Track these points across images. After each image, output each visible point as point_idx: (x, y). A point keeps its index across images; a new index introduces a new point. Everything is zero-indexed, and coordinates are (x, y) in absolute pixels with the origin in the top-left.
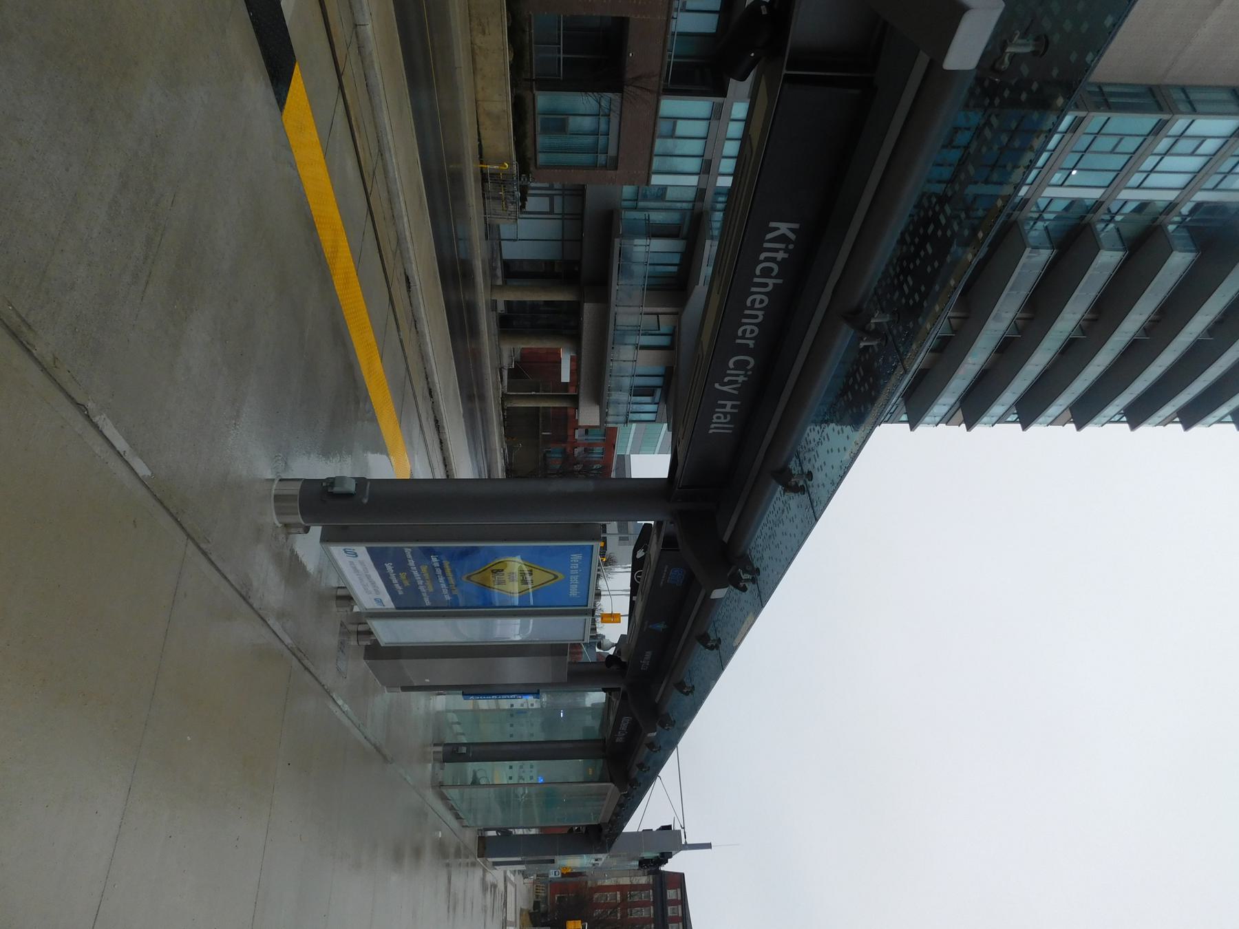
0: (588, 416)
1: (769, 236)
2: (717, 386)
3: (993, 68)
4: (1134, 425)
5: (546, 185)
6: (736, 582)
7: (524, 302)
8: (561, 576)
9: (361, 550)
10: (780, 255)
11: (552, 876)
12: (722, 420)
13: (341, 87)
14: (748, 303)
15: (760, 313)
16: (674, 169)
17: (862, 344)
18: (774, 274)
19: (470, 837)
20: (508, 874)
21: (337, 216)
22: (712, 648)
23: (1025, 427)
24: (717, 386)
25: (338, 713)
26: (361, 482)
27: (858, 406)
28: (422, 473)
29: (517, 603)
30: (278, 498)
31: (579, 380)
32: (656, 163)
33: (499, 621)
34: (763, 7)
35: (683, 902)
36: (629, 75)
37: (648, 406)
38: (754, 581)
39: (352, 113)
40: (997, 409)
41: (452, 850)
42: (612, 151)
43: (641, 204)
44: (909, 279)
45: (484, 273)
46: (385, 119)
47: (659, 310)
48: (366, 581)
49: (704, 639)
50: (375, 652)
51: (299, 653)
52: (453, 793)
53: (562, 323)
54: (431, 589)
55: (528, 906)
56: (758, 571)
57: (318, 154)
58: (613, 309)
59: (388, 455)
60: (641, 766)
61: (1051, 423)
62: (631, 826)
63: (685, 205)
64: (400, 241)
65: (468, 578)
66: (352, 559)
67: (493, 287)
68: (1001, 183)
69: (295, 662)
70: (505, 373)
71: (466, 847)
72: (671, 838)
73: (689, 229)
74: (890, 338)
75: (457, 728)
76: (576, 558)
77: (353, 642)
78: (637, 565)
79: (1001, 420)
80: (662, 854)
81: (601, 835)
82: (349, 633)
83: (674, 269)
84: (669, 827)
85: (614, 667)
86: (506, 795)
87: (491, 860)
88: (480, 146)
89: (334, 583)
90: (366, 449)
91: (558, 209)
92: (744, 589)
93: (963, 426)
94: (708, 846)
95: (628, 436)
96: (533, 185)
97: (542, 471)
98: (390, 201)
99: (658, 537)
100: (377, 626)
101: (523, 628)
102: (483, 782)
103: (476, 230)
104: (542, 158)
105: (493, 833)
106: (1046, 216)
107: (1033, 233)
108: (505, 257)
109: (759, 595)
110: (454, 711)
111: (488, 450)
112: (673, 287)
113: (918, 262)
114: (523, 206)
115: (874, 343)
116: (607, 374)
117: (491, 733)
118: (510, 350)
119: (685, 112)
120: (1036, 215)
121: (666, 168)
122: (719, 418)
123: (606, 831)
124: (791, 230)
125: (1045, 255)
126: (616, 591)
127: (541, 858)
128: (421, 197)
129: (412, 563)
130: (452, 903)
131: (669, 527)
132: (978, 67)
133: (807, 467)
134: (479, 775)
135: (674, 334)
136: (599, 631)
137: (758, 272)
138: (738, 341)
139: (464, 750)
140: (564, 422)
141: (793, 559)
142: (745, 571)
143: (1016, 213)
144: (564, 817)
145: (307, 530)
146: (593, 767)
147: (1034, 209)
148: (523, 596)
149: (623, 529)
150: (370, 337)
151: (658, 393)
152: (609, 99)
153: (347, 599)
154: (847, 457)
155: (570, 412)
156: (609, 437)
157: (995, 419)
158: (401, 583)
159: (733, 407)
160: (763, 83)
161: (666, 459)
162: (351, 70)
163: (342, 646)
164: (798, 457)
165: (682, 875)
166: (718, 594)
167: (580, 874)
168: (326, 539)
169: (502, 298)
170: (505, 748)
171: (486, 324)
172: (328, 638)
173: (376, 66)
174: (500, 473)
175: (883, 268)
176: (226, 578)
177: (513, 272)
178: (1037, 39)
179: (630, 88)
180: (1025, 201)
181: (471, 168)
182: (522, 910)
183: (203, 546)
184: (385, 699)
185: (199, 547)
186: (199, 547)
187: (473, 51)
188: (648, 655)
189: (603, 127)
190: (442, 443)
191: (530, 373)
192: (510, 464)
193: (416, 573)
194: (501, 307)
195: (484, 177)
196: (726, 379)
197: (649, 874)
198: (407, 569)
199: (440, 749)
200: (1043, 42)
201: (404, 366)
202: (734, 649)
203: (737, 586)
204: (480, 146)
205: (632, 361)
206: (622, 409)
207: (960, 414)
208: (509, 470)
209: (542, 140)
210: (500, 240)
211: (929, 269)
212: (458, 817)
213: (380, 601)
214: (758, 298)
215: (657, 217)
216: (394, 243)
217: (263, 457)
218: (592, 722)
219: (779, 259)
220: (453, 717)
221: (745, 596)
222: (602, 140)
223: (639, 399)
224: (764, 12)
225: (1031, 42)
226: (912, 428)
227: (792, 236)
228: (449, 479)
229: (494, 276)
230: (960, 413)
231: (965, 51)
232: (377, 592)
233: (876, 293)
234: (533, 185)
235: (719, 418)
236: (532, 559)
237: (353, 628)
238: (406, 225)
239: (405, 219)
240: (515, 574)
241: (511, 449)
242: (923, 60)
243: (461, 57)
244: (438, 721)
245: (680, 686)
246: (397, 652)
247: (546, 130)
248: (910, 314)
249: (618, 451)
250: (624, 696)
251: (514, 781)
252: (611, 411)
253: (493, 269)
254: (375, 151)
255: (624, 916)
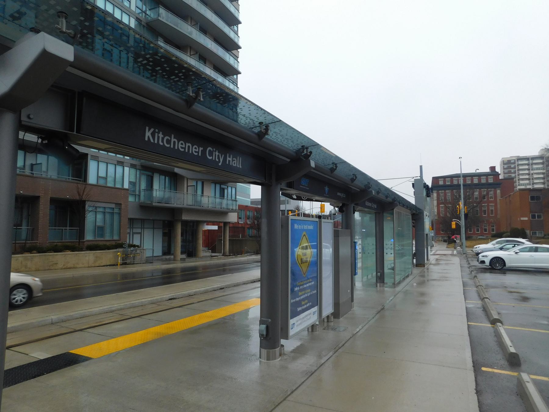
0: (233, 218)
1: (152, 141)
2: (220, 164)
3: (74, 37)
4: (238, 22)
5: (128, 235)
6: (308, 156)
7: (182, 246)
8: (304, 233)
9: (291, 321)
10: (161, 135)
11: (433, 234)
12: (236, 162)
13: (81, 330)
14: (183, 150)
15: (187, 145)
16: (121, 178)
17: (202, 99)
18: (169, 139)
19: (416, 271)
20: (432, 253)
21: (141, 332)
22: (336, 167)
23: (240, 23)
24: (220, 164)
25: (363, 330)
26: (261, 322)
27: (230, 100)
28: (258, 292)
29: (316, 250)
30: (268, 359)
31: (216, 222)
32: (118, 186)
33: (323, 258)
34: (44, 142)
35: (444, 178)
36: (77, 198)
37: (229, 191)
38: (307, 148)
39: (94, 325)
40: (232, 35)
41: (422, 279)
42: (113, 206)
43: (137, 193)
44: (172, 78)
45: (168, 264)
46: (96, 310)
47: (186, 186)
48: (305, 319)
49: (333, 170)
50: (336, 314)
51: (337, 348)
52: (398, 278)
53: (191, 229)
54: (309, 290)
55: (445, 245)
56: (303, 146)
57: (113, 341)
58: (185, 206)
59: (250, 309)
60: (387, 197)
61: (238, 11)
62: (412, 200)
63: (138, 173)
64: (153, 303)
65: (304, 274)
66: (295, 326)
67: (175, 260)
68: (128, 37)
69: (340, 350)
70: (213, 254)
71: (420, 273)
72: (418, 184)
73: (149, 172)
74: (199, 87)
75: (370, 276)
76: (296, 226)
77: (332, 324)
78: (299, 198)
79: (236, 33)
80: (424, 187)
81: (416, 214)
82: (328, 326)
83: (167, 178)
84: (413, 184)
85: (344, 209)
86: (399, 254)
87: (426, 261)
88: (110, 265)
89: (306, 333)
90: (247, 319)
91: (139, 230)
92: (311, 152)
93: (239, 50)
94: (421, 167)
95: (242, 200)
96: (128, 242)
97: (257, 238)
98: (135, 307)
99: (286, 190)
100: (325, 314)
101: (327, 247)
102: (393, 265)
103: (149, 267)
104: (116, 237)
105: (415, 260)
106: (144, 9)
107: (152, 16)
108: (161, 255)
109: (313, 146)
110: (362, 278)
111: (248, 263)
112: (175, 180)
113: (164, 74)
114: (138, 246)
115: (201, 94)
116: (214, 209)
117: (372, 261)
118: (203, 252)
119: (95, 171)
120: (144, 14)
121: (121, 181)
122: (234, 163)
123: (414, 212)
124: (149, 130)
125: (162, 11)
126: (311, 207)
127: (425, 244)
128: (134, 293)
129: (297, 299)
130: (445, 279)
131: (283, 185)
132: (72, 45)
133: (257, 124)
134: (390, 267)
135: (197, 180)
136: (328, 214)
137: (168, 146)
138: (200, 155)
139: (379, 274)
140: (236, 229)
141: (298, 131)
142: (303, 152)
143: (143, 23)
144: (408, 229)
145: (282, 346)
146: (387, 217)
147: (141, 15)
148: (312, 247)
149: (284, 203)
150: (196, 317)
151: (223, 186)
152: (88, 206)
153: (313, 327)
154: (253, 107)
155: (231, 225)
156: (242, 208)
157: (236, 36)
158: (306, 304)
159: (230, 157)
160: (79, 142)
161: (252, 186)
162: (74, 325)
163: (334, 329)
164: (253, 128)
165: (433, 178)
166: (313, 164)
167: (432, 222)
168: (286, 337)
169: (180, 256)
170: (378, 256)
171: (191, 263)
172: (331, 335)
173: (72, 314)
174: (258, 257)
175: (167, 89)
176: (303, 382)
177: (168, 251)
178: (59, 17)
179: (83, 197)
180: (138, 20)
181: (120, 270)
182: (447, 247)
183: (289, 393)
184: (357, 309)
185: (289, 395)
186: (289, 395)
187: (64, 269)
188: (339, 194)
189: (101, 210)
190: (245, 283)
191: (213, 242)
192: (254, 252)
193: (302, 297)
194: (184, 256)
195: (124, 264)
196: (217, 160)
197: (432, 192)
198: (300, 301)
199: (378, 285)
200: (60, 14)
201: (210, 301)
202: (337, 157)
203: (310, 156)
204: (110, 265)
205: (209, 198)
206: (230, 202)
207: (234, 52)
208: (257, 253)
209: (107, 238)
210: (153, 256)
211: (168, 69)
212: (408, 276)
213: (314, 313)
214: (181, 146)
215: (143, 186)
216: (154, 305)
217: (250, 365)
218: (367, 217)
219: (162, 136)
220: (365, 279)
221: (314, 151)
222: (107, 210)
223: (226, 195)
224: (46, 142)
225: (61, 19)
226: (240, 73)
227: (152, 130)
228: (261, 280)
229: (169, 260)
230: (233, 52)
231: (66, 51)
232: (310, 314)
233: (178, 93)
234: (128, 242)
235: (234, 163)
236: (296, 244)
237: (326, 324)
238: (146, 300)
239: (143, 300)
240: (303, 251)
241: (247, 252)
242: (70, 69)
243: (69, 274)
244: (367, 285)
245: (353, 180)
246: (337, 305)
247: (102, 235)
248: (189, 75)
249: (249, 204)
250: (357, 204)
251: (393, 252)
252: (231, 207)
253: (166, 260)
254: (111, 314)
255: (450, 203)
